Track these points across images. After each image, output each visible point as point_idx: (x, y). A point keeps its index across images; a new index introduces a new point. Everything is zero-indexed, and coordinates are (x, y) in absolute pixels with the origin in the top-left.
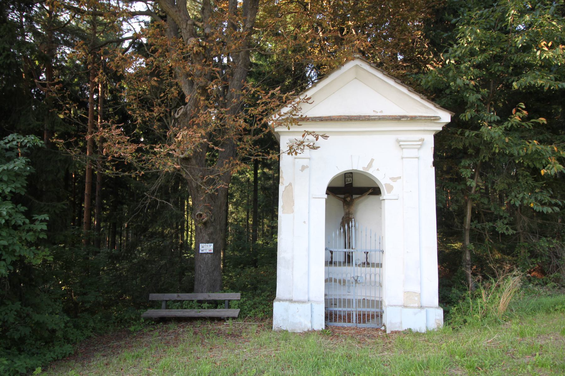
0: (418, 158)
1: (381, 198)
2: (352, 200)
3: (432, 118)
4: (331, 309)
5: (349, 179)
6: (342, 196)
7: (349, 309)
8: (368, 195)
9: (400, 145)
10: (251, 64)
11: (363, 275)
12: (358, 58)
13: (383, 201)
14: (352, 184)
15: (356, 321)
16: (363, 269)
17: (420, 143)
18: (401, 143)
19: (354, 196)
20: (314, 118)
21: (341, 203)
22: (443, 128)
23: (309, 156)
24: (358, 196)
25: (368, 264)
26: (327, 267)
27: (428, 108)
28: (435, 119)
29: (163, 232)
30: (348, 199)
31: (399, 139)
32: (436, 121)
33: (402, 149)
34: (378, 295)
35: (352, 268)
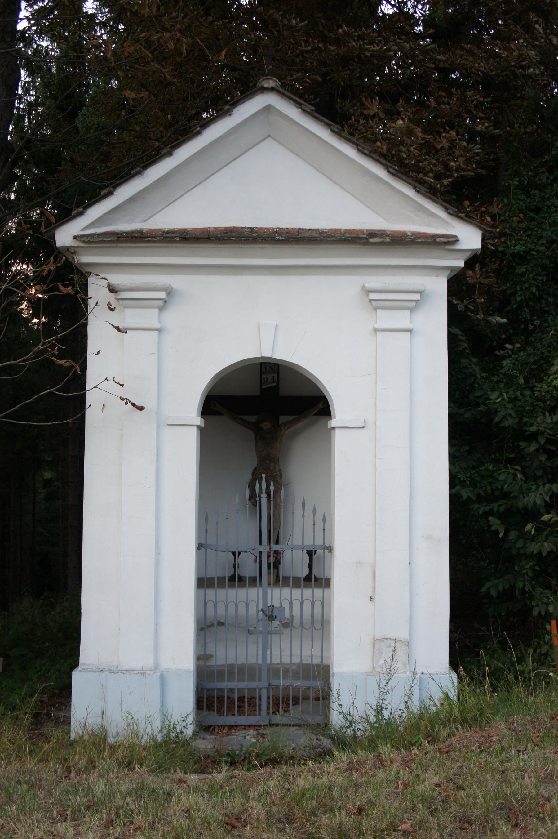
0: (410, 331)
1: (333, 423)
2: (277, 427)
3: (442, 239)
4: (210, 685)
5: (270, 377)
6: (252, 419)
7: (252, 685)
8: (315, 414)
9: (371, 301)
10: (32, 64)
11: (286, 605)
12: (272, 89)
13: (333, 431)
14: (277, 388)
15: (268, 708)
16: (232, 592)
17: (417, 297)
18: (372, 296)
19: (283, 419)
20: (169, 232)
21: (251, 434)
22: (466, 263)
23: (158, 326)
24: (290, 418)
25: (241, 579)
26: (202, 591)
27: (432, 215)
28: (451, 241)
29: (524, 41)
30: (266, 425)
31: (366, 285)
32: (448, 247)
33: (376, 309)
34: (317, 653)
35: (261, 590)
